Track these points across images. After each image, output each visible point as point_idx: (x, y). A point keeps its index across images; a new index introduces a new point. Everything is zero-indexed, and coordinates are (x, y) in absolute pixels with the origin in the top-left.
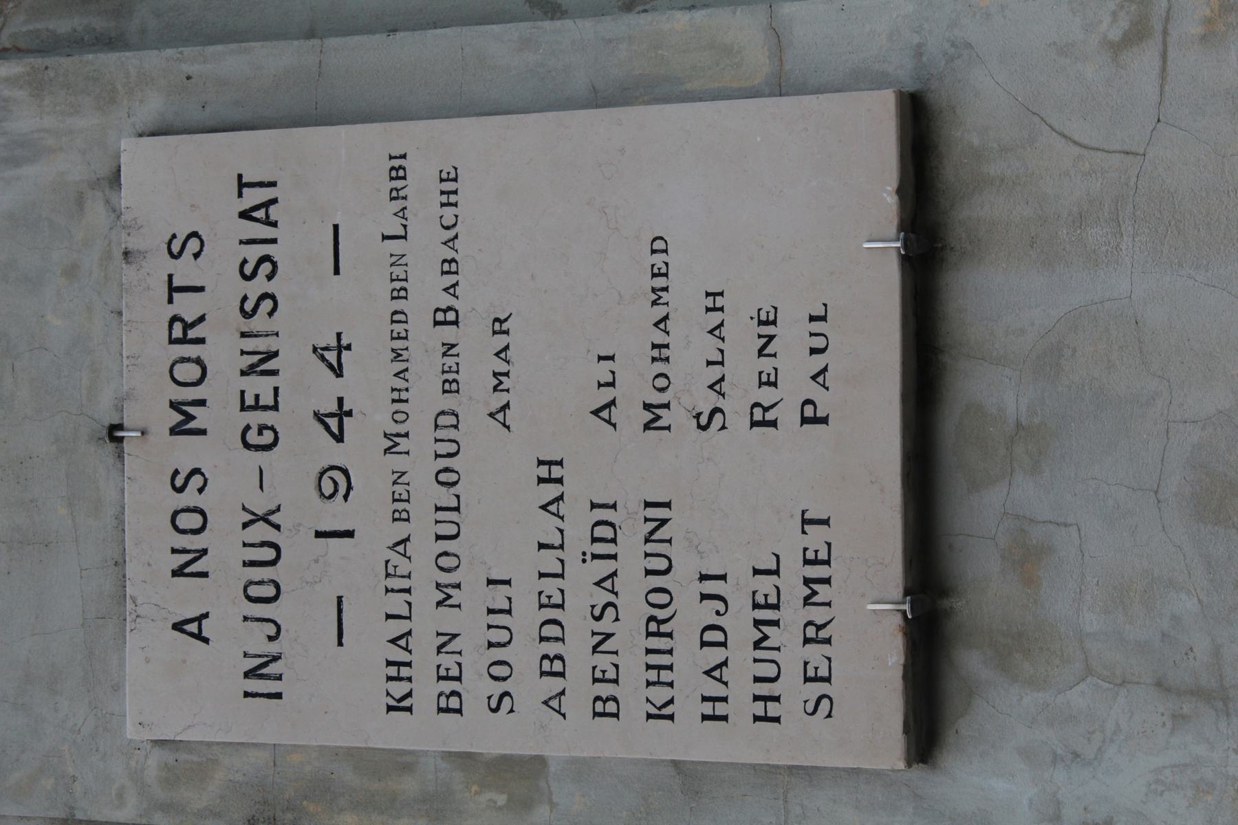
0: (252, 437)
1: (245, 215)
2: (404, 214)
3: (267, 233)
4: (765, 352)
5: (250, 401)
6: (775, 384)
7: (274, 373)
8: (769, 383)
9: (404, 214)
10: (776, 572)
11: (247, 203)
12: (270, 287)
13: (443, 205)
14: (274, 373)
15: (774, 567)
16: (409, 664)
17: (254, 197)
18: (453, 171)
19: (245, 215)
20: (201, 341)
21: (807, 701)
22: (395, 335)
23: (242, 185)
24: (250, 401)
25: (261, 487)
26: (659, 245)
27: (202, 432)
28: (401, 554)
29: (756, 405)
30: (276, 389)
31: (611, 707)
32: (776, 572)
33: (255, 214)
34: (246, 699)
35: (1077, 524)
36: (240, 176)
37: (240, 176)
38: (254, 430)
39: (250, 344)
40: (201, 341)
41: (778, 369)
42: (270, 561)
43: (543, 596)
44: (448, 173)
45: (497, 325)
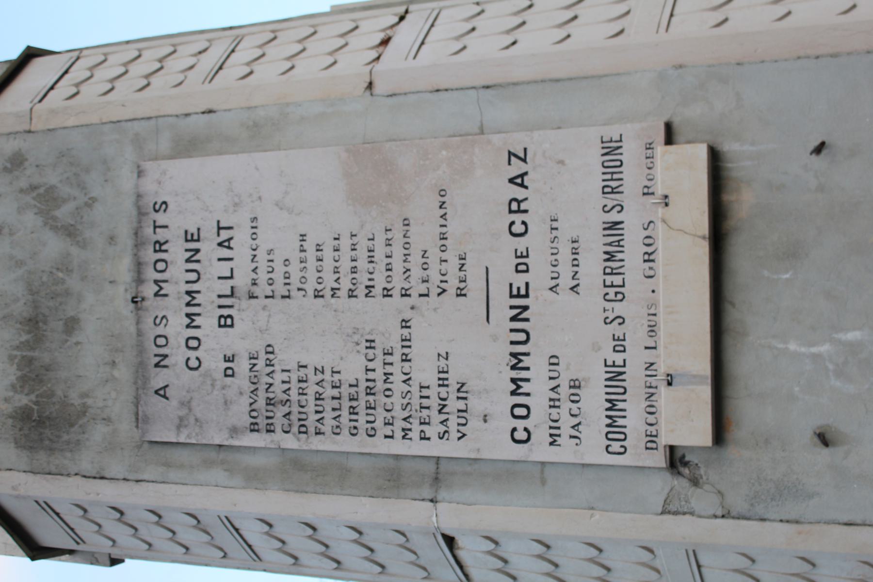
17: (225, 234)
27: (166, 295)
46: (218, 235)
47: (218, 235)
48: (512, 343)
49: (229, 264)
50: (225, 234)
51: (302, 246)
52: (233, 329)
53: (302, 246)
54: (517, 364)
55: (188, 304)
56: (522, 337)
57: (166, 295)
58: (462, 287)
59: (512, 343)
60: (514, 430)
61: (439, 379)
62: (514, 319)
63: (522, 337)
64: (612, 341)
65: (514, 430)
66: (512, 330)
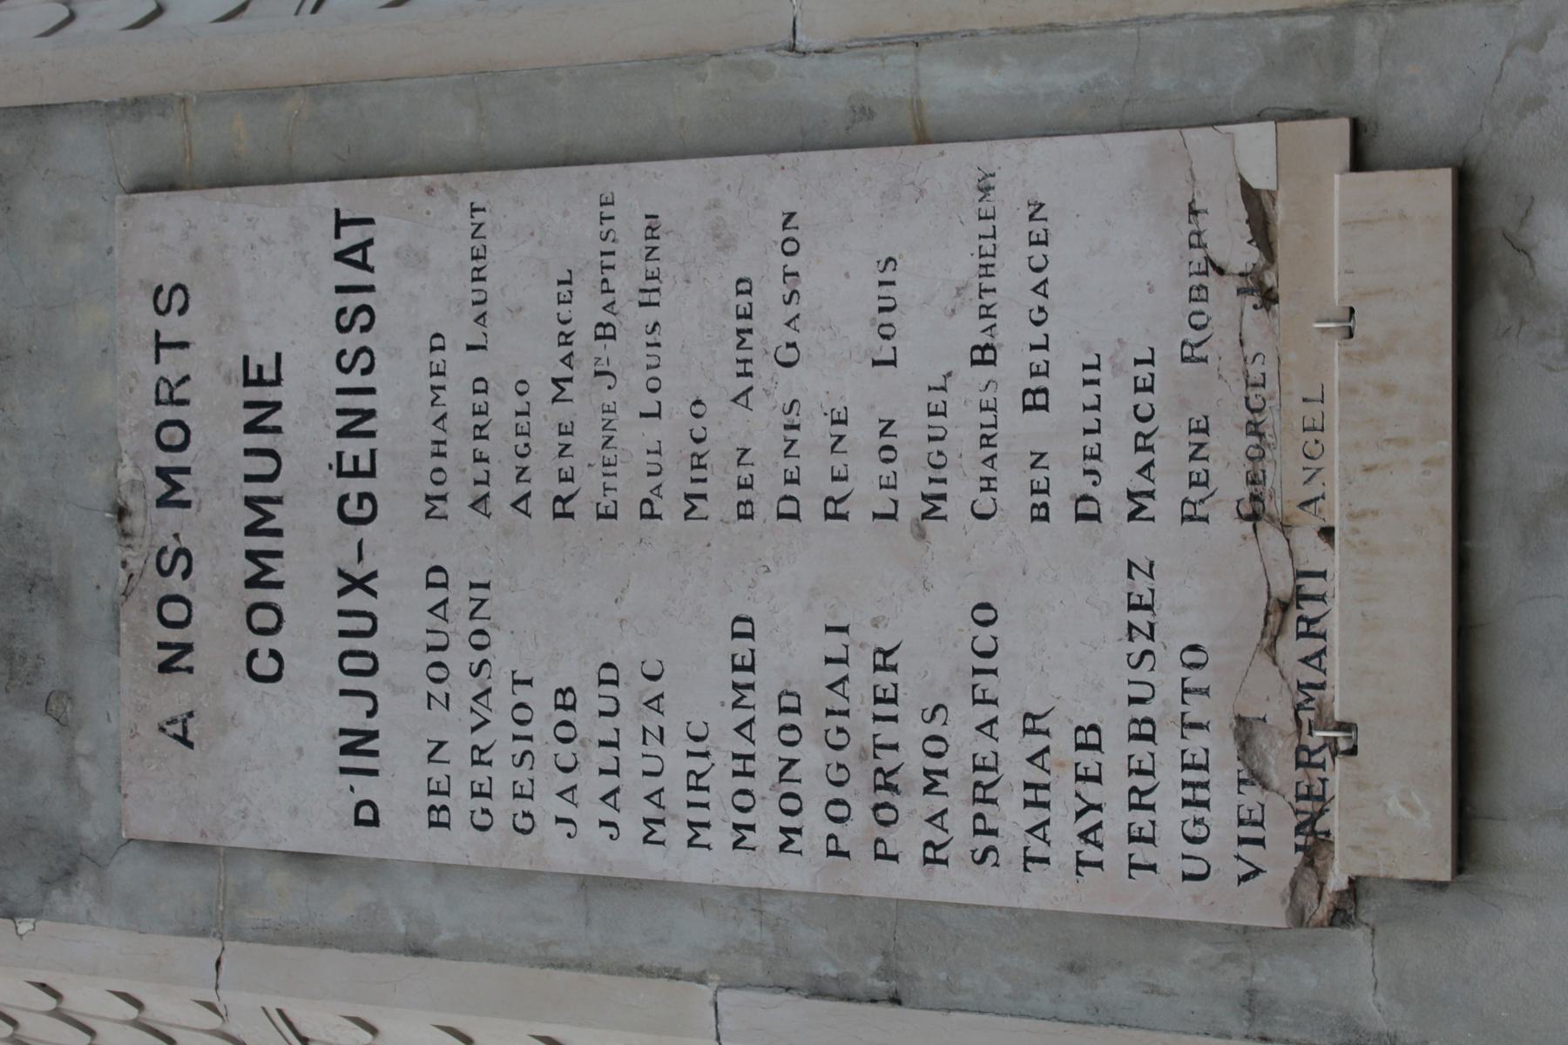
0: (351, 509)
1: (340, 256)
3: (360, 277)
4: (886, 433)
5: (348, 466)
6: (572, 480)
7: (371, 434)
8: (566, 480)
9: (993, 464)
10: (1046, 347)
11: (343, 244)
12: (367, 340)
14: (371, 434)
15: (1045, 343)
17: (351, 235)
19: (340, 256)
21: (1032, 257)
23: (340, 223)
24: (348, 466)
25: (1323, 413)
26: (744, 286)
27: (186, 504)
30: (373, 452)
31: (1040, 399)
32: (1046, 347)
38: (353, 500)
41: (277, 388)
43: (517, 786)
46: (337, 236)
47: (337, 236)
48: (249, 478)
49: (1094, 389)
50: (351, 235)
51: (605, 281)
52: (340, 608)
53: (605, 281)
54: (260, 522)
55: (251, 530)
56: (267, 465)
57: (186, 504)
58: (1146, 432)
59: (249, 478)
60: (253, 654)
61: (1185, 784)
62: (251, 428)
63: (267, 465)
64: (649, 490)
65: (253, 654)
66: (248, 452)
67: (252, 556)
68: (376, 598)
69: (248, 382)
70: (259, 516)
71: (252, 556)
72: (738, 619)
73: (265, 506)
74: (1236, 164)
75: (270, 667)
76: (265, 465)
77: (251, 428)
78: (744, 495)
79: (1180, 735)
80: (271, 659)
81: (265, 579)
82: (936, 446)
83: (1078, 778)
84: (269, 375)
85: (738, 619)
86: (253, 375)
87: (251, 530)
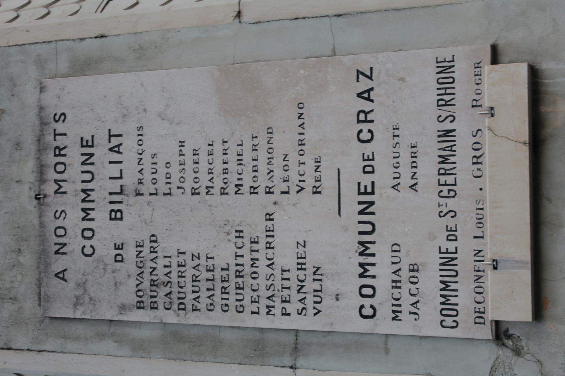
1: (111, 150)
2: (64, 276)
13: (393, 287)
16: (400, 282)
18: (256, 238)
19: (111, 150)
20: (65, 155)
22: (477, 269)
27: (65, 193)
28: (302, 246)
29: (267, 187)
33: (115, 149)
34: (457, 281)
35: (171, 166)
36: (439, 203)
37: (439, 203)
39: (482, 259)
40: (65, 155)
42: (59, 164)
44: (254, 239)
45: (210, 170)
48: (360, 233)
55: (84, 201)
56: (369, 228)
60: (362, 307)
62: (361, 213)
63: (369, 228)
65: (362, 307)
67: (83, 210)
68: (369, 271)
69: (82, 146)
70: (86, 196)
71: (83, 210)
72: (394, 245)
73: (88, 192)
74: (260, 22)
75: (370, 312)
76: (88, 177)
77: (361, 213)
78: (225, 166)
79: (438, 251)
80: (371, 309)
81: (366, 274)
82: (396, 160)
83: (252, 242)
84: (369, 190)
85: (394, 245)
86: (362, 190)
87: (84, 201)
